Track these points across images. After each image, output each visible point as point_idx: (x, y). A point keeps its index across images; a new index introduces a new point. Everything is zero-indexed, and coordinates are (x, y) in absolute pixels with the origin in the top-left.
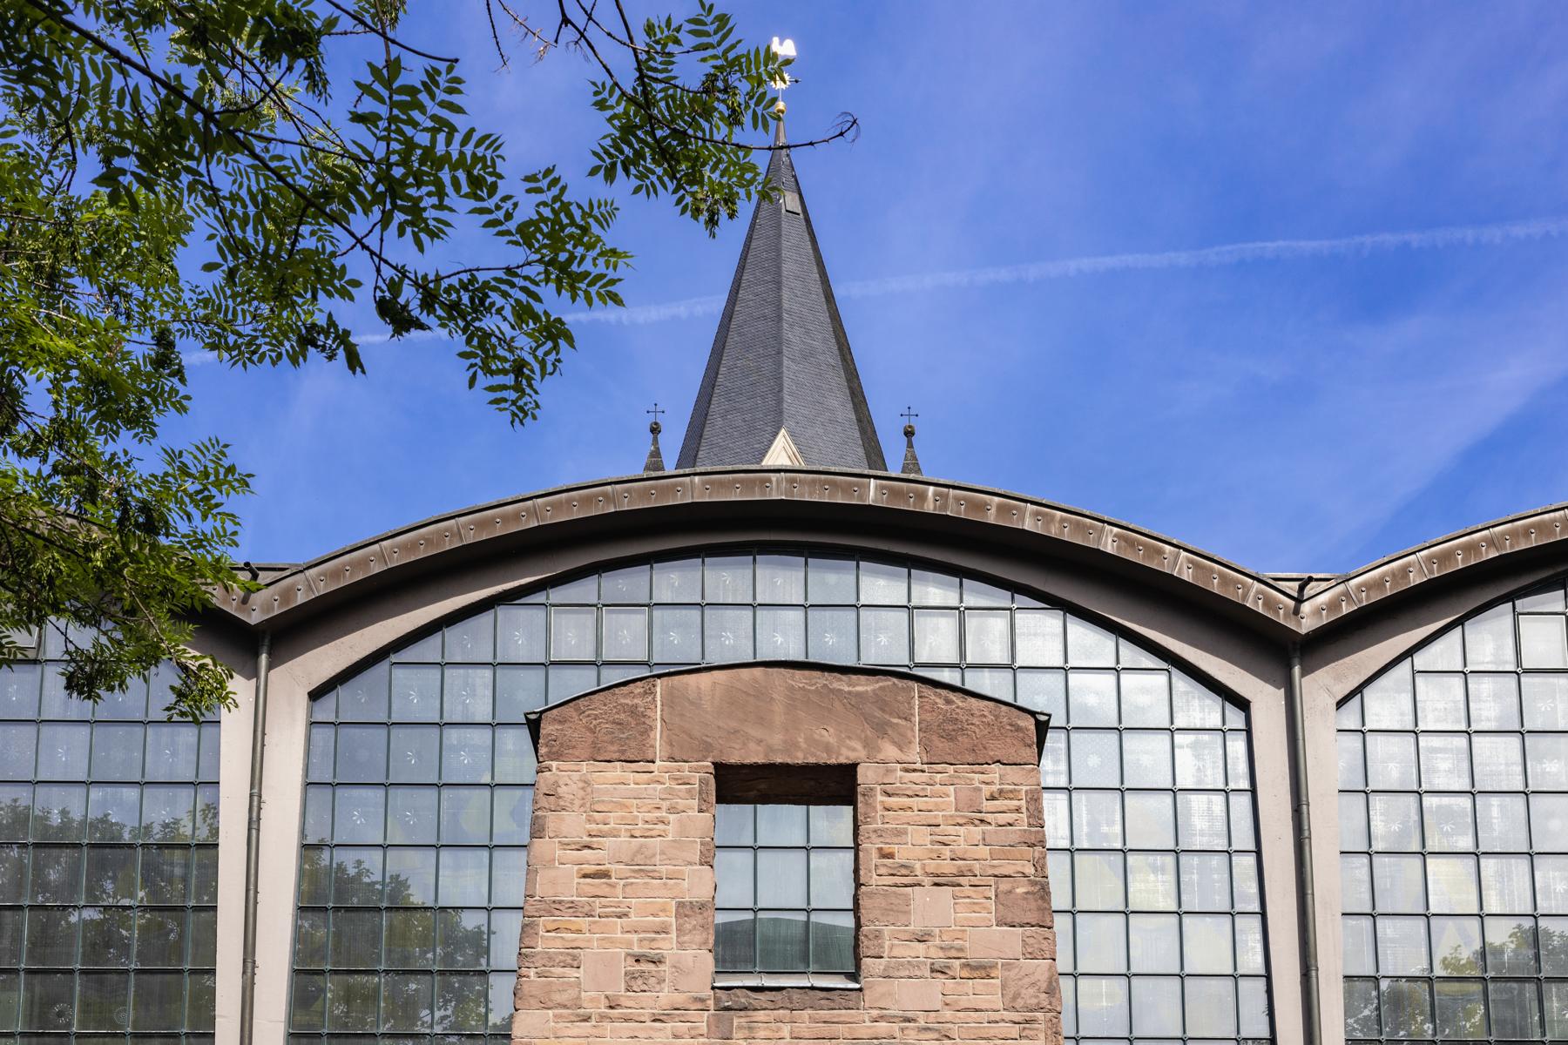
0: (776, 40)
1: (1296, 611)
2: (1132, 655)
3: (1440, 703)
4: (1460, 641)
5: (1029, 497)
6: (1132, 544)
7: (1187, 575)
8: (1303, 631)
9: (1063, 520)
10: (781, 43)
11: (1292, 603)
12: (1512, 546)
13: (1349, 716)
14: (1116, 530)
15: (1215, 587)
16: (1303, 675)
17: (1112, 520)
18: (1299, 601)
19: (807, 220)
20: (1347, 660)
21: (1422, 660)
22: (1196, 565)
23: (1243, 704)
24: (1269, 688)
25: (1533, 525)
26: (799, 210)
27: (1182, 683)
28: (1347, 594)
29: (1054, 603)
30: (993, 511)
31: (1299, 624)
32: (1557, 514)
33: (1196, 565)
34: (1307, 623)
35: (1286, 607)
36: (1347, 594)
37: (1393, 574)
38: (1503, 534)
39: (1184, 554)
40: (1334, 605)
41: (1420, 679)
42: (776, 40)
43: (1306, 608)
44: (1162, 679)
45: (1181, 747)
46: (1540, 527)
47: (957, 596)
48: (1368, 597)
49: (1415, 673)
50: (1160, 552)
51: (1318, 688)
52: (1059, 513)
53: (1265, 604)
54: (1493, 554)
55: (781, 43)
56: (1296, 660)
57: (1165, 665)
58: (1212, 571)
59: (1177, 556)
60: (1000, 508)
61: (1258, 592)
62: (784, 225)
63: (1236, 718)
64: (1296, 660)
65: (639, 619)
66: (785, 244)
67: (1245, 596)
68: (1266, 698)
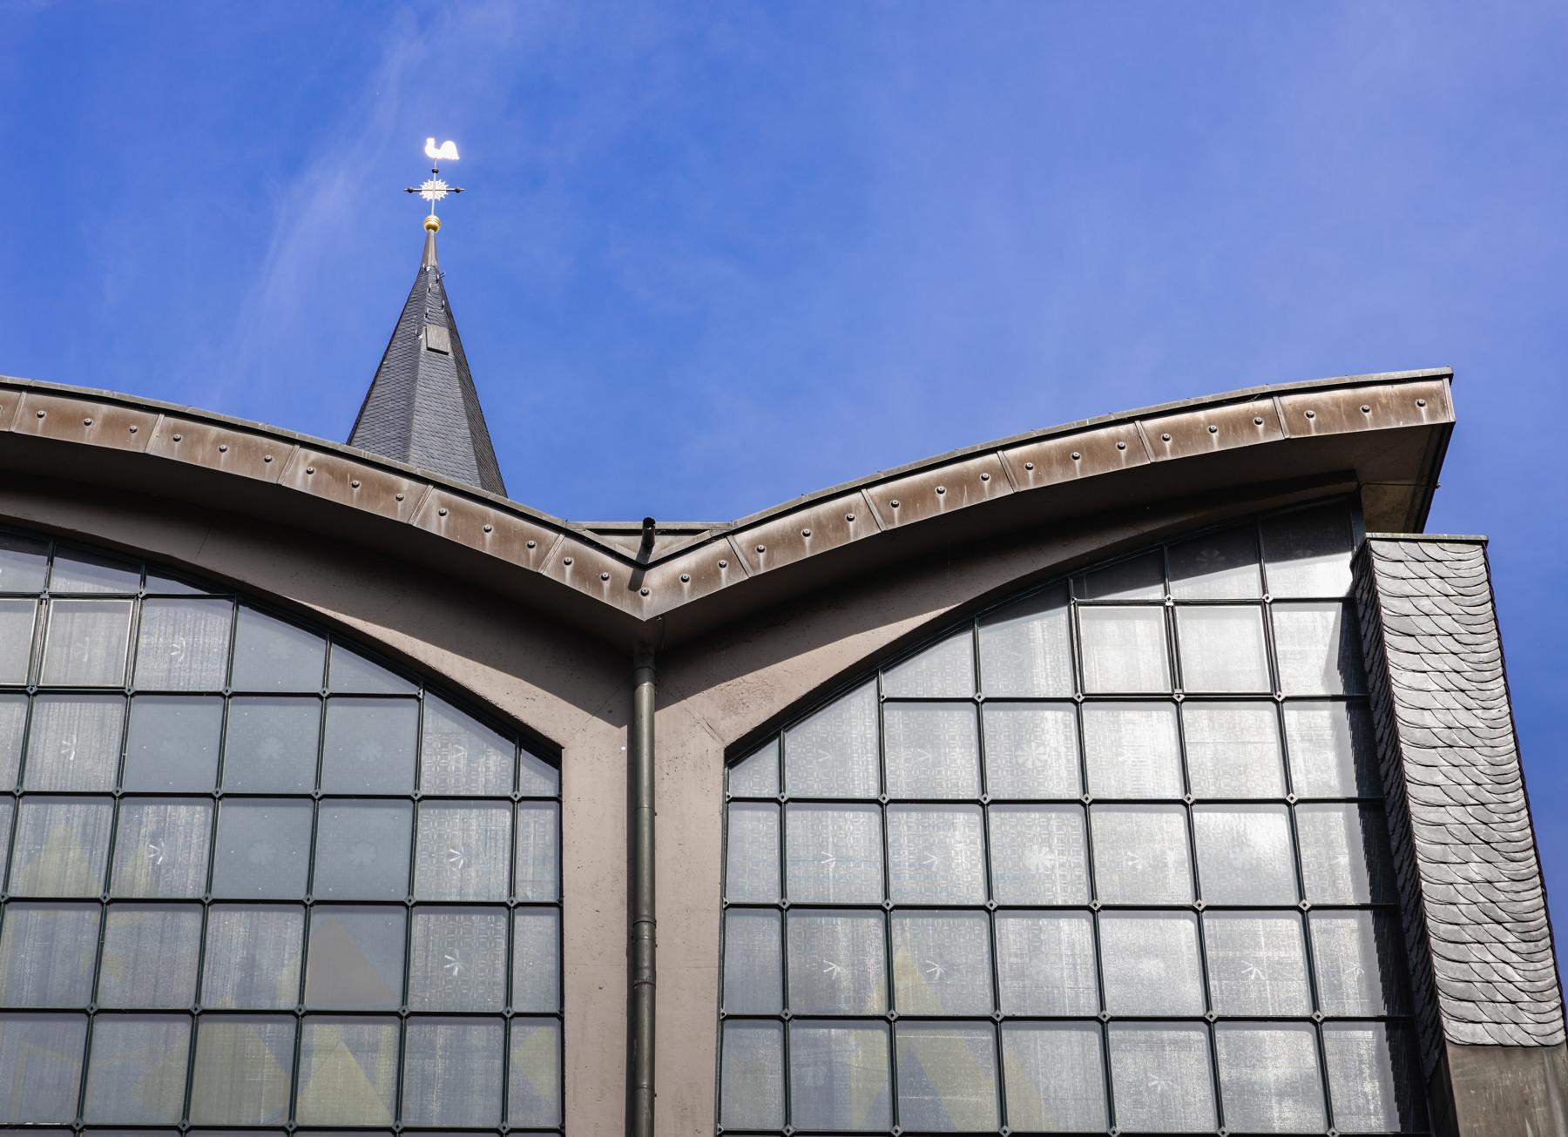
0: (431, 142)
1: (635, 584)
2: (352, 672)
3: (941, 755)
4: (969, 651)
5: (162, 404)
6: (341, 477)
7: (437, 526)
8: (644, 615)
9: (219, 440)
10: (438, 146)
11: (627, 571)
12: (1037, 478)
13: (758, 775)
14: (314, 455)
15: (487, 545)
16: (659, 703)
17: (309, 438)
18: (641, 566)
19: (462, 364)
20: (748, 677)
21: (897, 681)
22: (456, 511)
23: (549, 752)
24: (601, 725)
25: (1077, 447)
26: (448, 348)
27: (440, 719)
28: (731, 556)
29: (214, 586)
30: (96, 425)
31: (639, 604)
32: (1122, 429)
33: (456, 511)
34: (661, 593)
35: (616, 575)
36: (731, 556)
37: (819, 525)
38: (1022, 460)
39: (434, 493)
40: (706, 573)
41: (893, 715)
42: (431, 142)
43: (654, 578)
44: (408, 711)
45: (35, 658)
46: (1090, 450)
47: (42, 578)
48: (768, 561)
49: (883, 701)
50: (390, 489)
51: (694, 726)
52: (215, 430)
53: (576, 572)
54: (1004, 491)
55: (438, 146)
56: (646, 673)
57: (412, 689)
58: (485, 519)
59: (420, 497)
60: (109, 422)
61: (565, 553)
62: (421, 366)
63: (536, 780)
64: (646, 673)
65: (135, 878)
66: (420, 390)
67: (540, 560)
68: (591, 743)
